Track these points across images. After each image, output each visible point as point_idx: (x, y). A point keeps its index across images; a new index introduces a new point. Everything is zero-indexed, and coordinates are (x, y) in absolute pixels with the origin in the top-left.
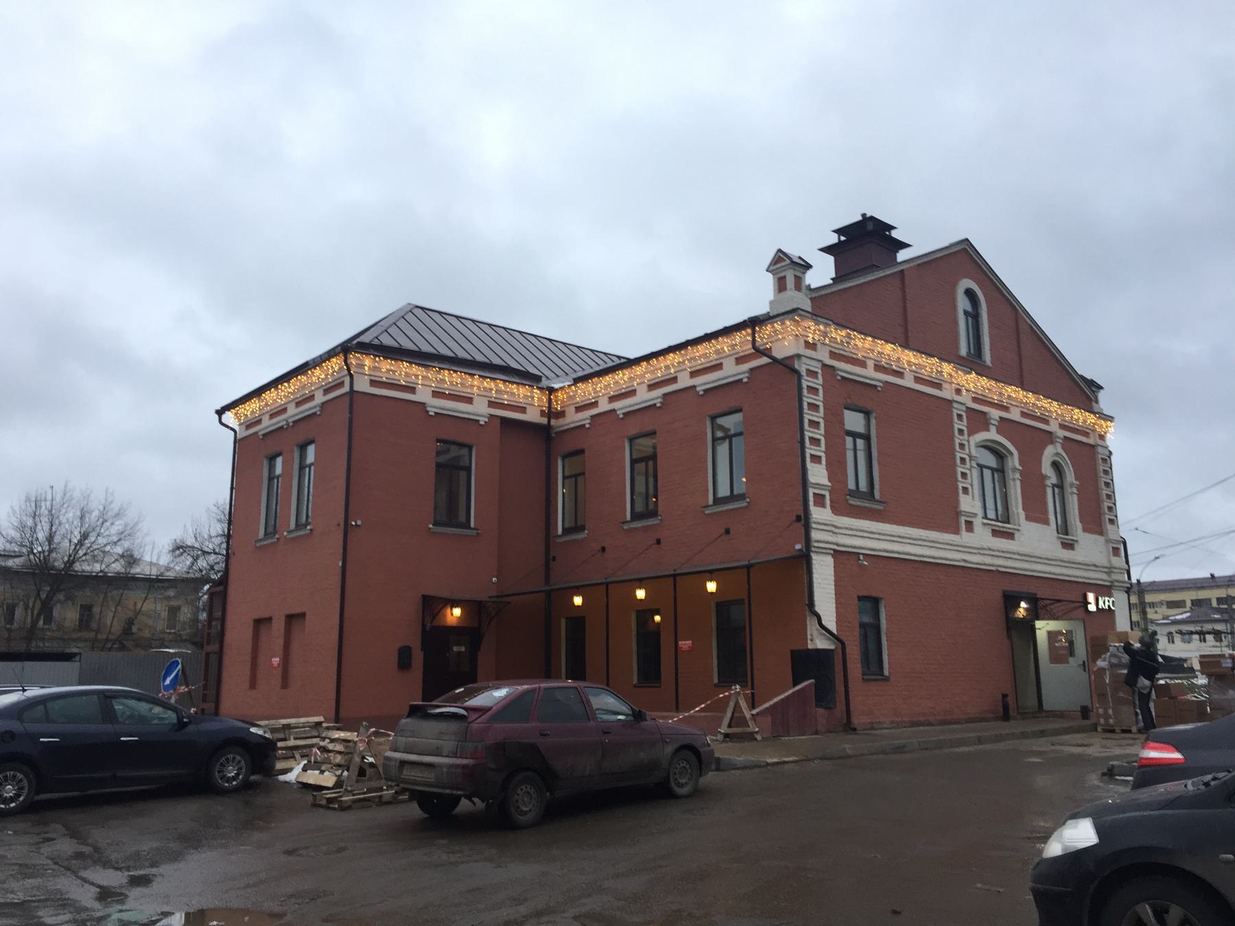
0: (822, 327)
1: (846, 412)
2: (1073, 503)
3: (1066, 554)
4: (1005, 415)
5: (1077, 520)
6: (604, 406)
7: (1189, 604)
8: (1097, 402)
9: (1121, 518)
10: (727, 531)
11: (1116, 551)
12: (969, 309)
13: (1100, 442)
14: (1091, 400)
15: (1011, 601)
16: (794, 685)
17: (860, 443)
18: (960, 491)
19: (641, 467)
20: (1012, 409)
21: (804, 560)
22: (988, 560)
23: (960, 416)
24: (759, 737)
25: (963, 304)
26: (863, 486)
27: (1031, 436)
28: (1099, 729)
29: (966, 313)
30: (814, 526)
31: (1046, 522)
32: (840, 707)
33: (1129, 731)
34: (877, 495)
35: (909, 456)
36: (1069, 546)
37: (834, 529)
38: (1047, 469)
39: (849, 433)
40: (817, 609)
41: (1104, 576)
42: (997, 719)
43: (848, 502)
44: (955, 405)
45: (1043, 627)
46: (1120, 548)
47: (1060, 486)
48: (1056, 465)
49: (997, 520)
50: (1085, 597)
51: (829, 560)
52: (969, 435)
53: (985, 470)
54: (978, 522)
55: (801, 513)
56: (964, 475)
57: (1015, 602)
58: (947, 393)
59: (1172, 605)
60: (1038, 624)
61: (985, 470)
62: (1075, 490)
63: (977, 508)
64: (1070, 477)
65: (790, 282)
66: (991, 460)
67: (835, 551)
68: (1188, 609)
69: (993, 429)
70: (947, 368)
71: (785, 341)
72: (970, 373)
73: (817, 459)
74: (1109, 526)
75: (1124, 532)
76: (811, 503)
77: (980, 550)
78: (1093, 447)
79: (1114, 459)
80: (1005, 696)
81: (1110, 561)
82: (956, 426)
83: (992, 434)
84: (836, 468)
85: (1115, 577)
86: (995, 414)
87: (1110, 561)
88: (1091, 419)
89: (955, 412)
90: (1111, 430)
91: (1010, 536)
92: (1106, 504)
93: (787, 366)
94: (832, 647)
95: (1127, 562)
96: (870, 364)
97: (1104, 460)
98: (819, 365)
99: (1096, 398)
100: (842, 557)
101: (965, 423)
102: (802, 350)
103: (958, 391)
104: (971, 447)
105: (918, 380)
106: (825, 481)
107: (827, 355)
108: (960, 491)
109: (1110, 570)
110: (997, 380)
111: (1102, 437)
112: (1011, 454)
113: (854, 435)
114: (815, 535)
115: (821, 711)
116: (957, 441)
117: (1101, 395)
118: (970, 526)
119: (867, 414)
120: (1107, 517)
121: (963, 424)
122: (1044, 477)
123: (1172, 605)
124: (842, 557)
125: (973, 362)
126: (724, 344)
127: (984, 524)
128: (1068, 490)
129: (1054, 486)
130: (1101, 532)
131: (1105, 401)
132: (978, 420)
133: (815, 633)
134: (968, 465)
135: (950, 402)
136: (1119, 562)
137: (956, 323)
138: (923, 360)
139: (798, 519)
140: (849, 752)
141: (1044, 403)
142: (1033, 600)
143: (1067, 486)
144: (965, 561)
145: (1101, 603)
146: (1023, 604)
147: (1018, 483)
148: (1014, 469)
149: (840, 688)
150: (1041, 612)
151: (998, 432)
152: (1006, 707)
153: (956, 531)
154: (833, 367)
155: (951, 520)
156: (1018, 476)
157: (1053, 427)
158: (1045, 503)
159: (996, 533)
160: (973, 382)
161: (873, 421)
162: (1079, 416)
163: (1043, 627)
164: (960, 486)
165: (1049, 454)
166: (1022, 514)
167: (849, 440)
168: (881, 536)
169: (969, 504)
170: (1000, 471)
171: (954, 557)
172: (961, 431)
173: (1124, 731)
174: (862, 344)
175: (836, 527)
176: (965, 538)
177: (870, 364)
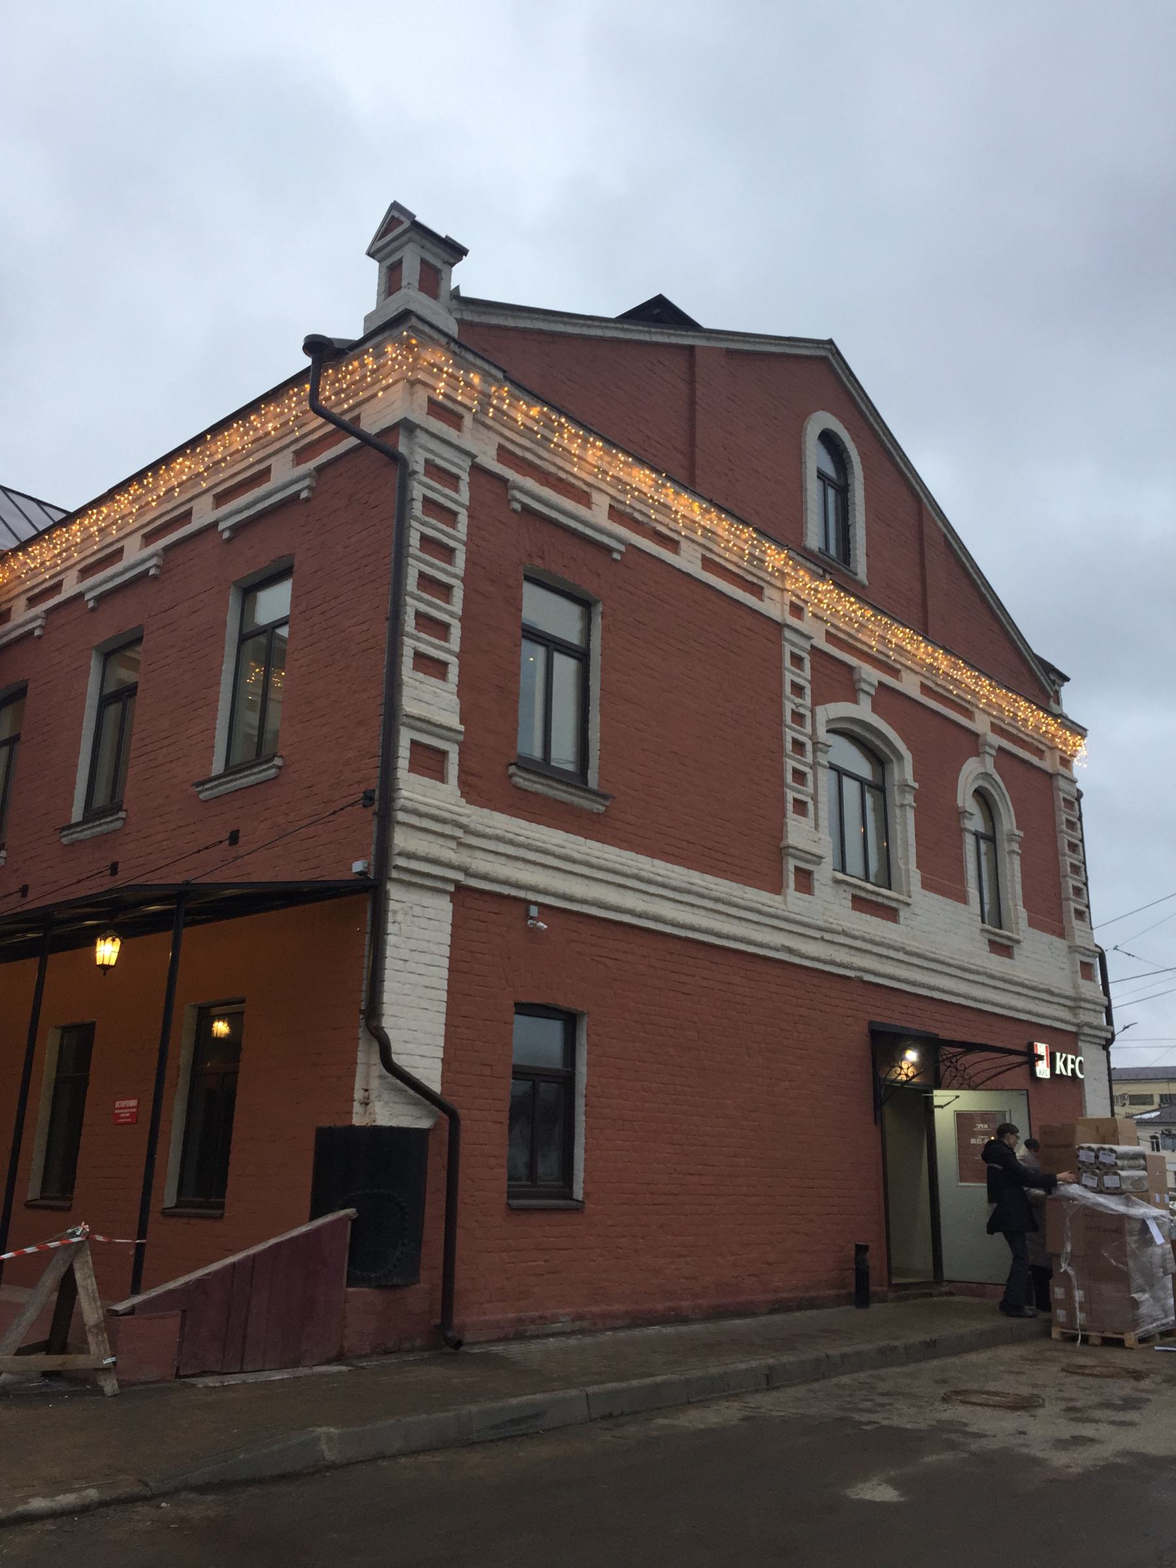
0: (476, 379)
1: (528, 589)
2: (1013, 870)
3: (996, 964)
4: (888, 680)
5: (1020, 903)
6: (71, 588)
7: (1157, 1100)
8: (1058, 702)
9: (1098, 913)
10: (234, 838)
11: (1086, 968)
12: (830, 470)
13: (1062, 770)
14: (1049, 697)
15: (885, 1043)
16: (313, 1218)
17: (565, 667)
18: (790, 806)
19: (113, 710)
20: (905, 674)
21: (369, 894)
22: (842, 956)
23: (797, 660)
24: (110, 1385)
25: (816, 458)
26: (564, 753)
27: (941, 736)
28: (1055, 1333)
29: (821, 475)
30: (401, 816)
31: (962, 898)
32: (430, 1276)
33: (1119, 1343)
34: (593, 779)
35: (687, 734)
36: (1002, 948)
37: (463, 835)
38: (965, 799)
39: (534, 635)
40: (387, 1023)
41: (1065, 1014)
42: (839, 1301)
43: (498, 773)
44: (787, 634)
45: (949, 1104)
46: (1093, 964)
47: (990, 838)
48: (981, 795)
49: (867, 879)
50: (1031, 1047)
51: (443, 908)
52: (815, 703)
53: (846, 781)
54: (824, 873)
55: (375, 784)
56: (799, 776)
57: (894, 1046)
58: (773, 607)
59: (1137, 1100)
60: (940, 1096)
61: (846, 781)
62: (1016, 847)
63: (825, 846)
64: (1008, 822)
65: (411, 272)
66: (864, 769)
67: (459, 886)
68: (1156, 1106)
69: (865, 702)
70: (775, 557)
71: (384, 398)
72: (822, 578)
73: (432, 666)
74: (1076, 923)
75: (1101, 938)
76: (403, 762)
77: (824, 933)
78: (1051, 776)
79: (1087, 806)
80: (861, 1250)
81: (1075, 986)
82: (788, 677)
83: (863, 710)
84: (489, 692)
85: (1084, 1017)
86: (871, 674)
87: (1075, 986)
88: (1050, 726)
89: (788, 649)
90: (1082, 752)
91: (889, 913)
92: (1071, 882)
93: (383, 451)
94: (425, 1124)
95: (1106, 992)
96: (601, 502)
97: (1069, 804)
98: (467, 464)
99: (1057, 692)
100: (481, 911)
101: (807, 673)
102: (419, 416)
103: (797, 610)
104: (817, 725)
105: (708, 564)
106: (454, 722)
107: (493, 452)
108: (790, 806)
109: (1076, 1003)
110: (877, 609)
111: (1066, 762)
112: (900, 758)
113: (553, 645)
114: (401, 840)
115: (361, 1295)
116: (788, 707)
117: (1065, 691)
118: (805, 880)
119: (586, 604)
120: (1073, 905)
121: (804, 676)
122: (962, 814)
123: (1137, 1100)
124: (481, 911)
125: (834, 565)
126: (268, 423)
127: (838, 882)
128: (1004, 846)
129: (978, 836)
130: (1061, 935)
131: (1072, 701)
132: (834, 677)
133: (375, 1084)
134: (809, 758)
135: (780, 626)
136: (1091, 989)
137: (801, 488)
138: (722, 526)
139: (368, 798)
140: (330, 1454)
141: (967, 676)
142: (931, 1046)
143: (1001, 838)
144: (790, 951)
145: (1059, 1064)
146: (912, 1056)
147: (910, 815)
148: (904, 786)
149: (433, 1233)
150: (947, 1076)
151: (874, 710)
152: (862, 1275)
153: (777, 888)
154: (504, 481)
155: (762, 858)
156: (909, 799)
157: (980, 725)
158: (960, 861)
159: (860, 903)
160: (825, 597)
161: (598, 621)
162: (1027, 715)
163: (949, 1104)
164: (790, 796)
165: (970, 773)
166: (916, 876)
167: (534, 656)
168: (593, 871)
169: (800, 833)
170: (878, 788)
171: (768, 939)
172: (798, 689)
173: (1108, 1342)
174: (588, 457)
175: (467, 830)
176: (793, 902)
177: (601, 502)
